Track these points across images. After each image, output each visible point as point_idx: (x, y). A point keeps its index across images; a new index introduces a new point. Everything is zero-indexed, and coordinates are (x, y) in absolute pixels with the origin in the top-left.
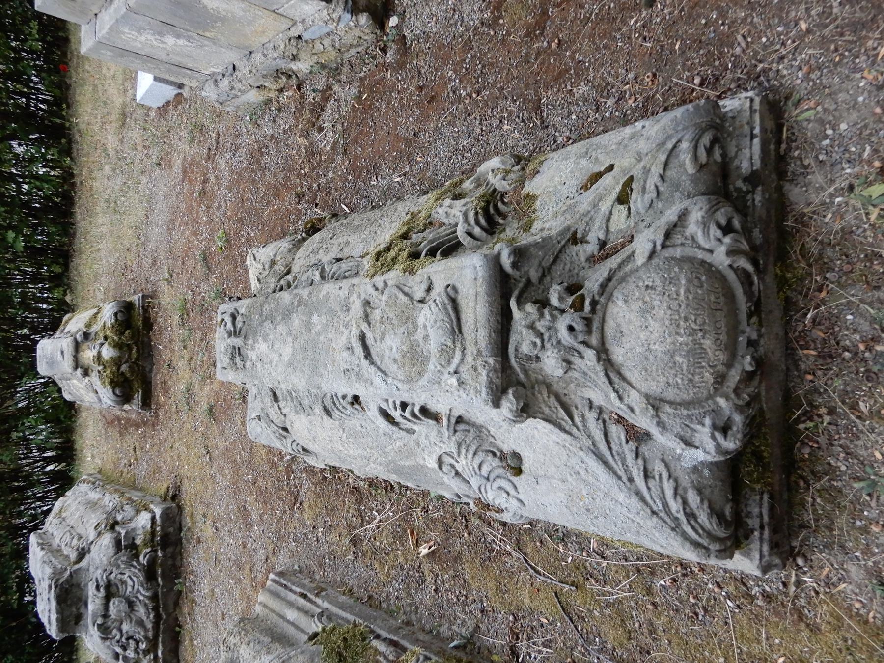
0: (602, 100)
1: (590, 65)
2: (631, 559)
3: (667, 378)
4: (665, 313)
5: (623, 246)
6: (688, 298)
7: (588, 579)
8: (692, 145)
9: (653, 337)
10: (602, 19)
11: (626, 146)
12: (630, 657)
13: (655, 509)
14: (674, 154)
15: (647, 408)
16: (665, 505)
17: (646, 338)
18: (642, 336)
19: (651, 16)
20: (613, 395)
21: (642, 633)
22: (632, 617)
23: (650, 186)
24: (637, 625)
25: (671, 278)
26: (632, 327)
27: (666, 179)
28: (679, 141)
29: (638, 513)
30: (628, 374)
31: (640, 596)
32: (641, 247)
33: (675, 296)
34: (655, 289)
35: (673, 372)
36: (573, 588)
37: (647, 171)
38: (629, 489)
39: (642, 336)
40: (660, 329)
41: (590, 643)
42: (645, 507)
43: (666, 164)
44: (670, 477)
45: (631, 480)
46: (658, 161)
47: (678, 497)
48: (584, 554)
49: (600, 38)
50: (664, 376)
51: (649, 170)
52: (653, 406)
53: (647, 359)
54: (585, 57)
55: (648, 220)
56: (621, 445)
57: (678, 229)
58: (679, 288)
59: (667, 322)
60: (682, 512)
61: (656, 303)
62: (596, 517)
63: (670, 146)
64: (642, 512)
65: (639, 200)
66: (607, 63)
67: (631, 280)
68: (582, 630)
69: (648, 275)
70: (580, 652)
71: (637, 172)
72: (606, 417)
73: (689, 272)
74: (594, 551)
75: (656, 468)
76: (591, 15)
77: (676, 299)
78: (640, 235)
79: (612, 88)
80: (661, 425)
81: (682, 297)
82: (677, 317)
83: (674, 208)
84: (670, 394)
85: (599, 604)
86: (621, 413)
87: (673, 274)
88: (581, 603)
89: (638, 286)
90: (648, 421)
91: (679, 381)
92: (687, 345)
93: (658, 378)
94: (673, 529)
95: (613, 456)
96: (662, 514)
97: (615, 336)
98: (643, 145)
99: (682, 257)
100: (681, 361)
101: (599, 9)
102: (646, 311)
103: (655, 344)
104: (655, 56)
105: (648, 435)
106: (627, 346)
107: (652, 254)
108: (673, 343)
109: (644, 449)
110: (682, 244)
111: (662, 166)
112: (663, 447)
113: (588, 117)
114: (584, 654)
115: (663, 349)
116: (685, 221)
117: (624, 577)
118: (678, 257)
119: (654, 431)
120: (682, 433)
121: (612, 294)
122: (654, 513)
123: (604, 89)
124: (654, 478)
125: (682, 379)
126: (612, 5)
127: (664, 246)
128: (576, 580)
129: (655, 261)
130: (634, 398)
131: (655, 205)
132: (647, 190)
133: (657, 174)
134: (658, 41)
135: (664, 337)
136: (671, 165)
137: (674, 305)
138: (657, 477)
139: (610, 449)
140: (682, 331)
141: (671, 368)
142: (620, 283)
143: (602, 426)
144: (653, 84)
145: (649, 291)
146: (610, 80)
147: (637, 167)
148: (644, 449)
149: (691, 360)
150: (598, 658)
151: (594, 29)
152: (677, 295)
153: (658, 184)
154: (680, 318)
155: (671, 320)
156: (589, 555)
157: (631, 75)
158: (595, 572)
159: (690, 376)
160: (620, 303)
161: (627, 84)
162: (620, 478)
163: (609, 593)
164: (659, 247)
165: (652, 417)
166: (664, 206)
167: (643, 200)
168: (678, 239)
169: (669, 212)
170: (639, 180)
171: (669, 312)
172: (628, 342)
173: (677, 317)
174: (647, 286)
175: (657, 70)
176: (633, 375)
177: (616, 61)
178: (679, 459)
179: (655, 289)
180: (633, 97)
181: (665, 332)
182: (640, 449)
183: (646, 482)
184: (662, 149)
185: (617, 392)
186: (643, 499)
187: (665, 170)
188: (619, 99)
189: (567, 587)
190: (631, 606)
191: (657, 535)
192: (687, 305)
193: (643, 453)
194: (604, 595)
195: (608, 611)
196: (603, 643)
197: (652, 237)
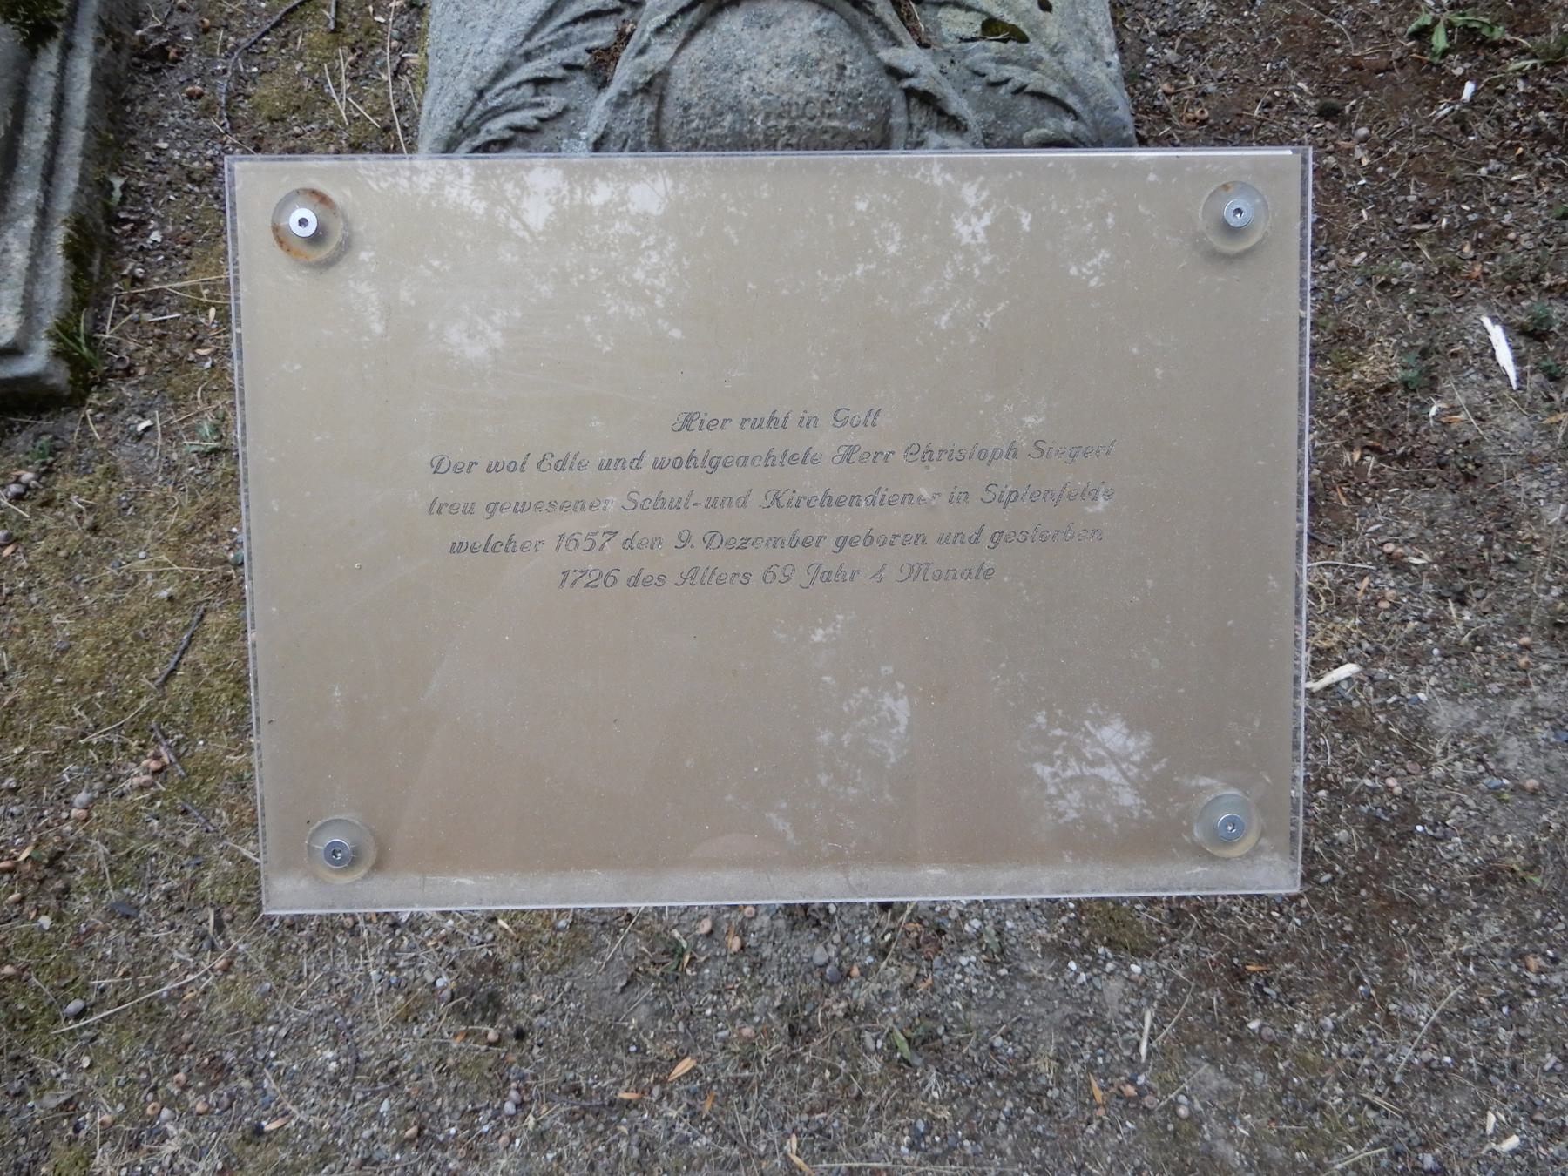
0: (1178, 41)
1: (1244, 18)
2: (403, 118)
3: (697, 104)
4: (800, 95)
5: (913, 31)
6: (825, 132)
7: (353, 51)
8: (1068, 137)
9: (762, 75)
10: (1320, 35)
11: (1080, 32)
12: (242, 123)
13: (488, 96)
14: (1058, 108)
15: (646, 73)
16: (495, 113)
17: (759, 64)
18: (762, 59)
19: (1302, 115)
20: (663, 17)
21: (285, 139)
22: (308, 123)
23: (1007, 71)
24: (297, 130)
25: (856, 107)
26: (776, 41)
27: (1018, 97)
28: (1077, 117)
29: (475, 68)
30: (699, 40)
31: (345, 135)
32: (908, 56)
33: (827, 111)
34: (838, 80)
35: (707, 112)
36: (332, 26)
37: (1033, 64)
38: (512, 53)
39: (762, 59)
40: (774, 86)
41: (246, 58)
42: (487, 78)
43: (1041, 96)
44: (542, 120)
45: (528, 57)
46: (1048, 81)
47: (512, 133)
48: (395, 43)
49: (1288, 34)
50: (700, 98)
51: (1035, 69)
52: (649, 83)
53: (726, 68)
54: (1259, 10)
55: (953, 71)
56: (583, 40)
57: (935, 118)
58: (840, 119)
59: (785, 98)
60: (489, 138)
61: (817, 80)
62: (457, 8)
63: (1071, 100)
64: (478, 74)
65: (988, 54)
66: (1242, 47)
67: (855, 43)
68: (265, 44)
69: (862, 71)
70: (225, 41)
71: (1035, 48)
72: (627, 14)
73: (866, 137)
74: (403, 59)
75: (553, 99)
76: (1333, 16)
77: (823, 113)
78: (928, 58)
79: (1196, 58)
80: (622, 101)
81: (826, 123)
82: (794, 114)
83: (970, 111)
84: (672, 112)
85: (315, 71)
86: (635, 36)
87: (863, 110)
88: (310, 40)
89: (844, 52)
90: (626, 78)
91: (694, 125)
92: (751, 132)
93: (695, 90)
94: (460, 124)
95: (564, 26)
96: (480, 107)
97: (760, 16)
98: (1076, 56)
99: (891, 128)
100: (725, 124)
101: (1339, 30)
102: (805, 65)
103: (750, 79)
104: (1235, 121)
105: (603, 84)
106: (745, 35)
107: (895, 73)
108: (752, 109)
109: (580, 80)
110: (910, 126)
111: (1038, 88)
112: (589, 110)
113: (1152, 19)
114: (224, 47)
115: (742, 93)
116: (948, 129)
117: (370, 108)
118: (891, 121)
119: (612, 92)
120: (613, 137)
121: (831, 9)
122: (481, 93)
123: (1197, 44)
124: (536, 94)
125: (697, 129)
126: (1339, 51)
127: (910, 93)
128: (347, 30)
129: (885, 82)
130: (661, 53)
131: (977, 80)
132: (1002, 67)
133: (1026, 81)
134: (1259, 127)
135: (761, 93)
136: (1039, 104)
137: (812, 110)
138: (538, 99)
139: (575, 21)
140: (772, 123)
141: (713, 108)
142: (850, 24)
143: (611, 6)
144: (1189, 121)
145: (836, 70)
146: (1211, 54)
147: (1042, 48)
148: (580, 80)
149: (728, 140)
150: (225, 71)
151: (1306, 23)
152: (830, 116)
153: (1010, 84)
154: (794, 119)
155: (789, 104)
156: (394, 51)
157: (1211, 87)
158: (369, 63)
159: (702, 142)
160: (817, 23)
161: (1198, 81)
162: (528, 37)
163: (338, 86)
164: (906, 83)
165: (634, 84)
166: (975, 95)
167: (985, 60)
168: (920, 118)
169: (965, 103)
170: (1020, 51)
171: (801, 101)
172: (752, 37)
173: (794, 114)
174: (843, 68)
175: (1211, 126)
176: (698, 49)
177: (1240, 62)
178: (571, 135)
179: (838, 80)
180: (1172, 90)
181: (770, 94)
182: (579, 74)
183: (527, 82)
184: (1066, 89)
185: (668, 24)
186: (499, 76)
187: (1033, 94)
188: (1173, 69)
189: (330, 15)
190: (326, 120)
191: (447, 99)
192: (813, 131)
193: (574, 78)
194: (333, 77)
195: (307, 84)
196: (252, 79)
197: (923, 72)
